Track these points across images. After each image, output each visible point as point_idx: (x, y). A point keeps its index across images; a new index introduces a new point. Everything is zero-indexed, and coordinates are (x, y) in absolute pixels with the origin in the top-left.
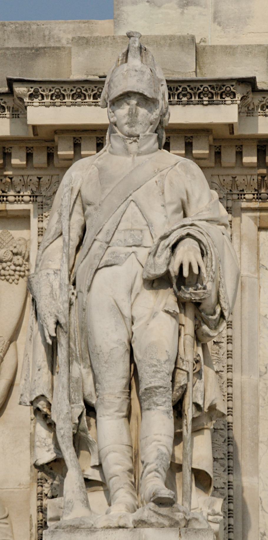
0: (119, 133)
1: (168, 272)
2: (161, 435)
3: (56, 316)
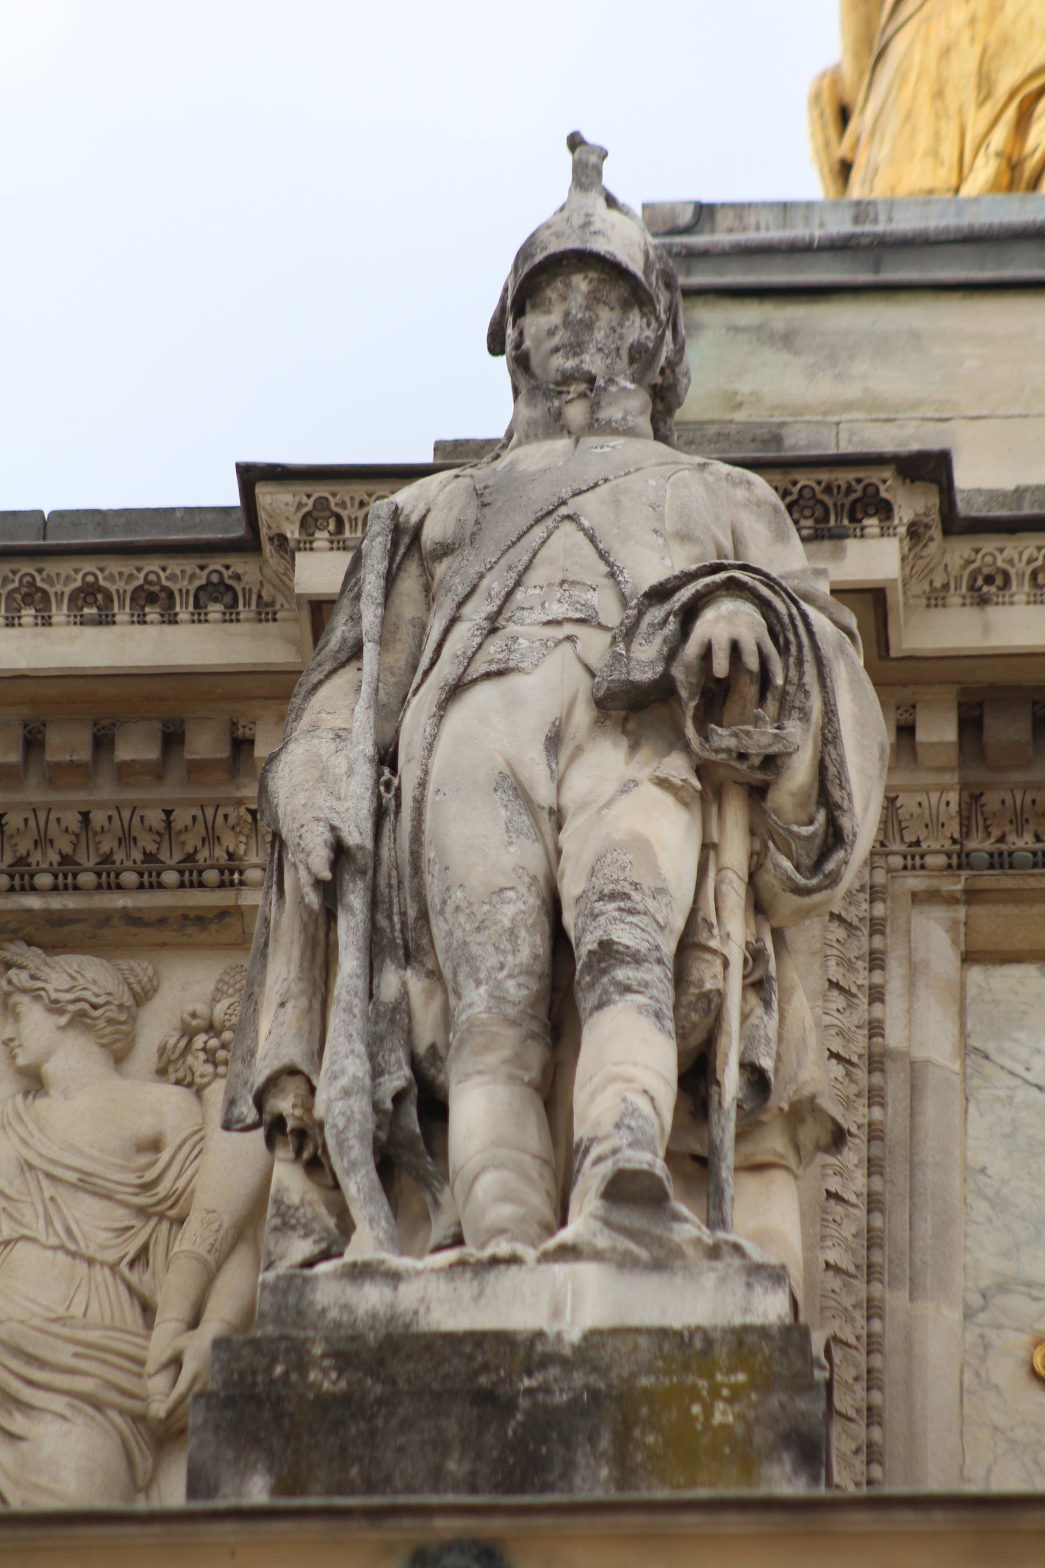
3: (333, 829)
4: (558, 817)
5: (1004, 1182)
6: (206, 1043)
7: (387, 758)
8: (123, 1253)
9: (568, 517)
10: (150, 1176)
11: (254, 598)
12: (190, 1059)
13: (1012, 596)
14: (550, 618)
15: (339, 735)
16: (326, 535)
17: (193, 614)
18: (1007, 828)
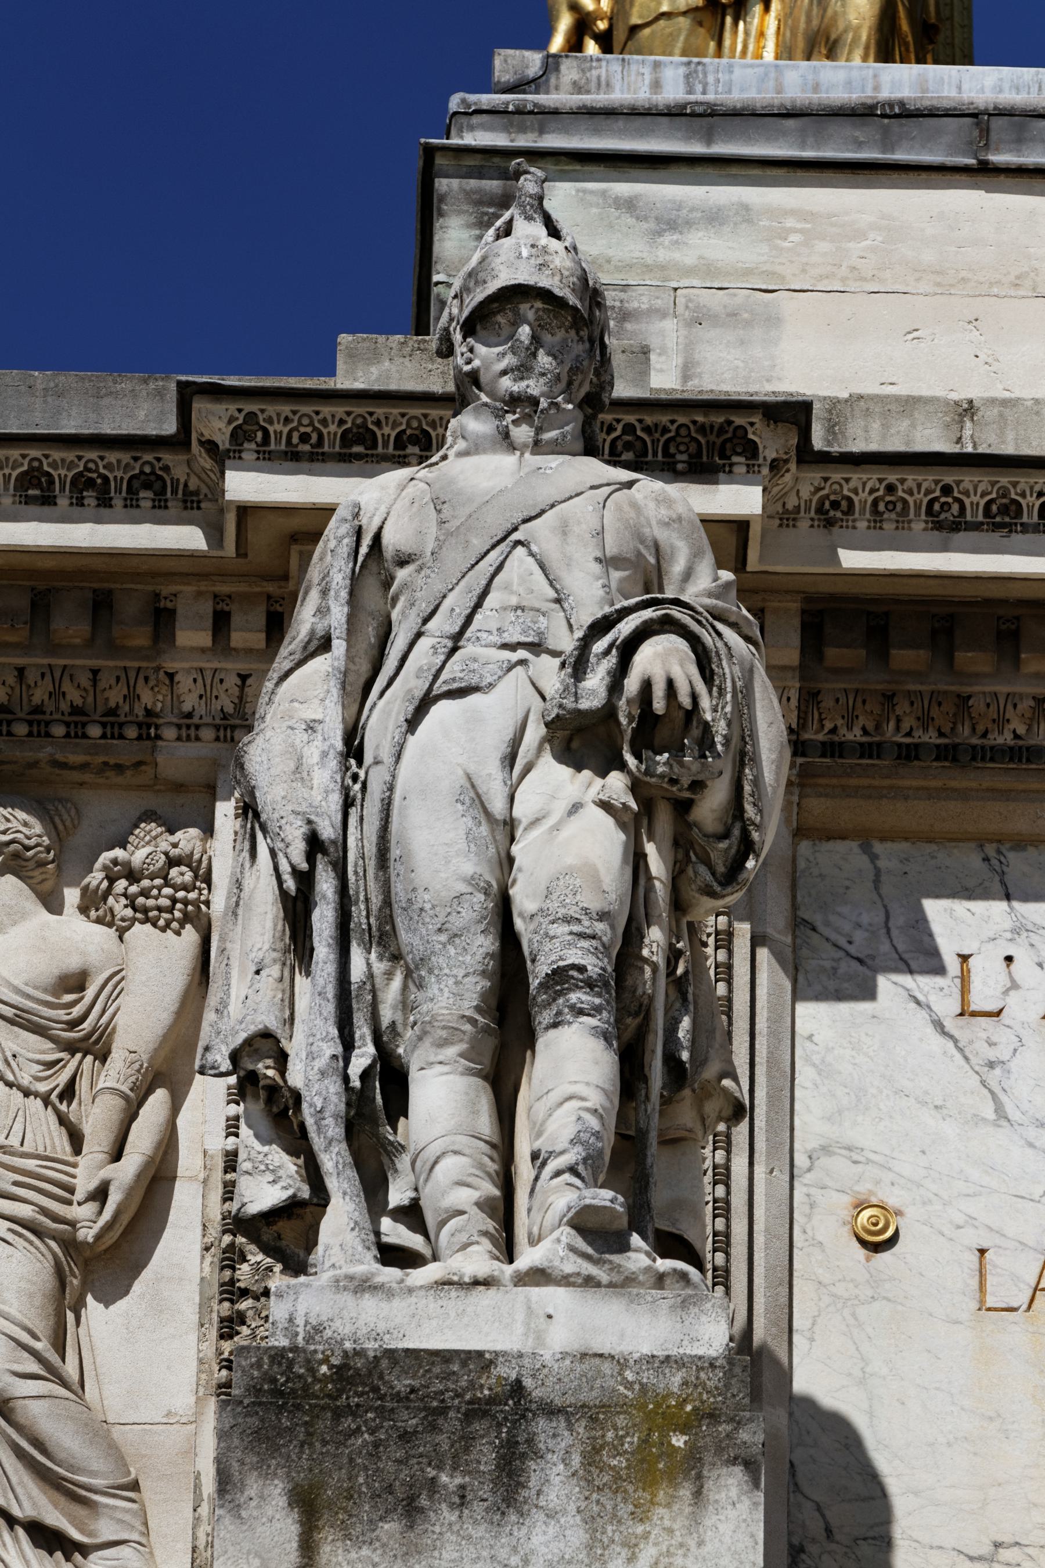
0: (484, 398)
1: (609, 711)
2: (588, 1084)
3: (309, 822)
4: (509, 828)
5: (829, 1050)
6: (126, 889)
7: (353, 747)
8: (52, 1086)
9: (518, 543)
10: (77, 1011)
11: (181, 487)
12: (111, 900)
13: (854, 521)
14: (504, 641)
15: (311, 727)
16: (253, 446)
17: (125, 499)
18: (840, 722)
